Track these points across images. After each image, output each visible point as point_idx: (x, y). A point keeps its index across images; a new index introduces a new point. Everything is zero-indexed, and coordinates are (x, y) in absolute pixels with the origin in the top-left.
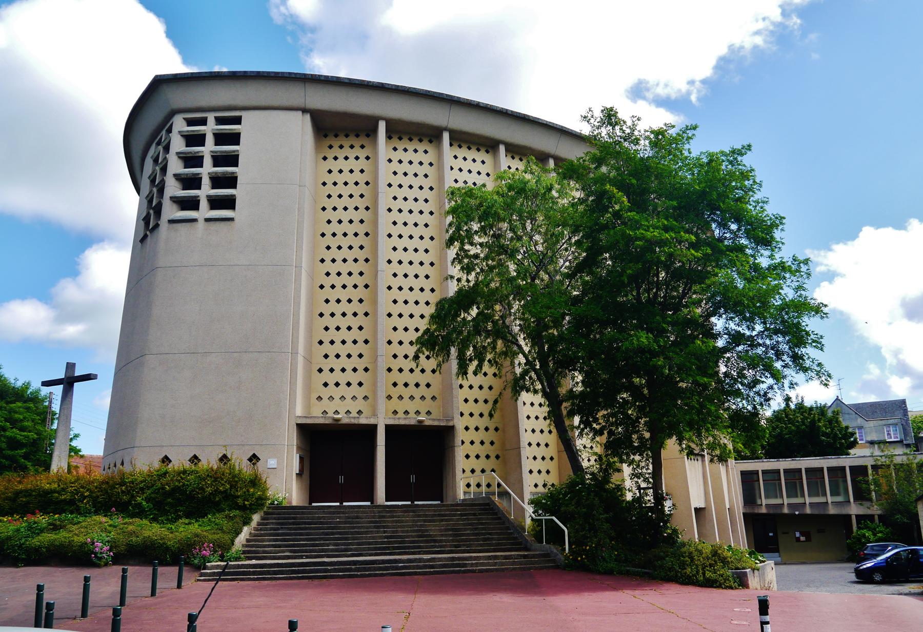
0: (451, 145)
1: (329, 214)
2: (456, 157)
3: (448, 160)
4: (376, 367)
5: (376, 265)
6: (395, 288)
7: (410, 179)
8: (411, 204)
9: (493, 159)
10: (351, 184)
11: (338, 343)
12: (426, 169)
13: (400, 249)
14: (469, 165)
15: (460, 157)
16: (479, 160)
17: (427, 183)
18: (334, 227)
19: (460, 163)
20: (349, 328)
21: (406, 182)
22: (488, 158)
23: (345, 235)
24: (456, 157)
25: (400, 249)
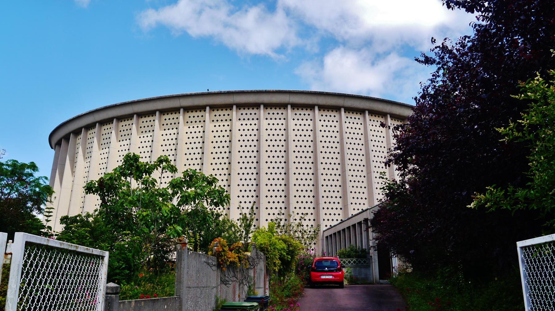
0: (345, 112)
13: (300, 202)
24: (347, 117)
25: (300, 202)
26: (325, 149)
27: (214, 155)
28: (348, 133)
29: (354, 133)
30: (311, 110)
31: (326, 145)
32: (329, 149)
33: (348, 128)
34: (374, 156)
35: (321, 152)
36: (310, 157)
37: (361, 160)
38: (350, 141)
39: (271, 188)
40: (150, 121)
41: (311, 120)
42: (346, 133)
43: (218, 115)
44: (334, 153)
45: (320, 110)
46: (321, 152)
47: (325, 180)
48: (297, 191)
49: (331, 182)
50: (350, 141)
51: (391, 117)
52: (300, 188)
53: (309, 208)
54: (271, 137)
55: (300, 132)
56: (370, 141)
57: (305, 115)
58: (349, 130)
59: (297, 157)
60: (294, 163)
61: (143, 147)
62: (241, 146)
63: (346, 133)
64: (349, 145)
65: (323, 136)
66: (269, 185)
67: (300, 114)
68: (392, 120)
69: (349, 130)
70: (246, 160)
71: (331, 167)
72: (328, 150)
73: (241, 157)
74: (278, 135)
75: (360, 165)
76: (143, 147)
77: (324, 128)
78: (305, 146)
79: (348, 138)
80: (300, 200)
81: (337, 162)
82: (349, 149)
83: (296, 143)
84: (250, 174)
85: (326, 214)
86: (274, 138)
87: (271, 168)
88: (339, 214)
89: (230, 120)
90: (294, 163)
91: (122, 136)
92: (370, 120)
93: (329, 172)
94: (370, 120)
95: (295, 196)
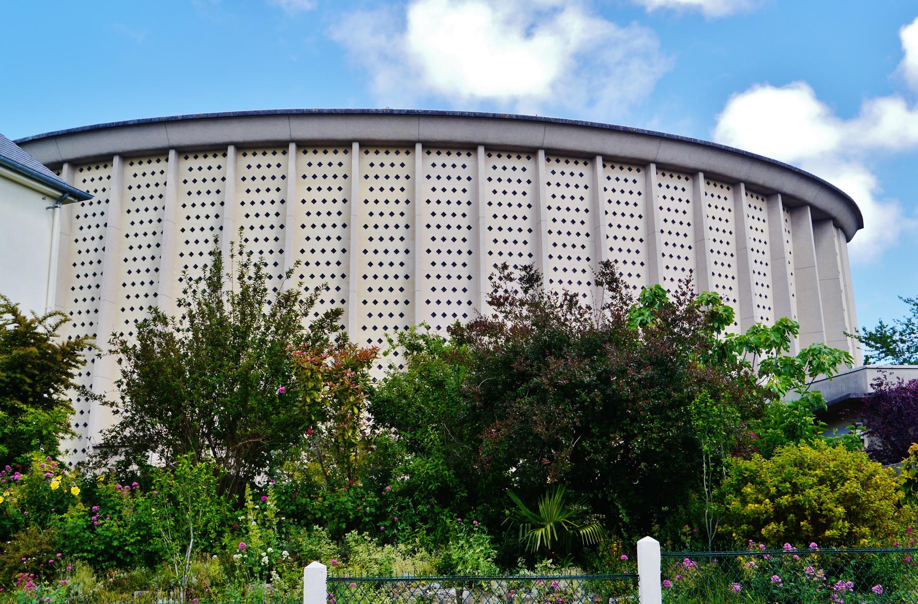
0: (604, 166)
1: (248, 208)
2: (609, 178)
3: (602, 182)
4: (478, 276)
5: (414, 232)
6: (371, 202)
7: (509, 198)
8: (449, 195)
9: (691, 187)
10: (381, 227)
11: (386, 265)
12: (581, 191)
13: (500, 241)
14: (621, 185)
15: (558, 172)
16: (577, 174)
17: (583, 206)
18: (313, 243)
19: (612, 184)
20: (386, 252)
21: (505, 200)
22: (687, 185)
23: (391, 264)
24: (609, 178)
25: (500, 241)
26: (558, 202)
27: (308, 230)
28: (610, 213)
29: (622, 192)
30: (529, 158)
31: (559, 216)
32: (567, 202)
33: (610, 201)
34: (667, 267)
35: (549, 208)
36: (525, 218)
37: (638, 252)
38: (614, 231)
39: (438, 234)
40: (153, 173)
41: (529, 182)
42: (606, 213)
43: (315, 164)
44: (579, 259)
45: (548, 160)
46: (549, 208)
47: (555, 245)
48: (495, 216)
49: (569, 251)
50: (614, 231)
51: (705, 177)
52: (500, 187)
53: (520, 230)
54: (439, 219)
55: (505, 234)
56: (658, 234)
57: (514, 169)
58: (613, 207)
59: (495, 192)
60: (490, 204)
61: (132, 309)
62: (371, 239)
63: (606, 213)
64: (610, 218)
65: (554, 220)
66: (434, 251)
67: (504, 168)
68: (708, 184)
69: (613, 207)
70: (381, 247)
71: (570, 265)
72: (564, 204)
73: (371, 239)
74: (454, 215)
75: (633, 239)
76: (132, 309)
77: (558, 202)
78: (515, 217)
79: (610, 225)
80: (500, 236)
81: (583, 230)
82: (611, 249)
83: (495, 209)
84: (391, 302)
85: (555, 269)
86: (443, 222)
87: (439, 289)
88: (582, 198)
89: (345, 176)
90: (490, 228)
91: (81, 228)
92: (660, 185)
93: (565, 228)
94: (660, 185)
95: (490, 204)
